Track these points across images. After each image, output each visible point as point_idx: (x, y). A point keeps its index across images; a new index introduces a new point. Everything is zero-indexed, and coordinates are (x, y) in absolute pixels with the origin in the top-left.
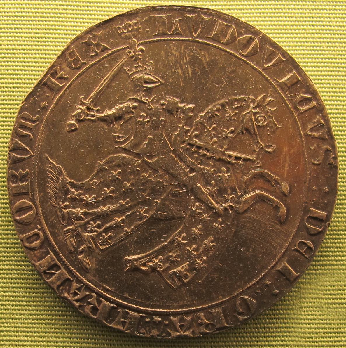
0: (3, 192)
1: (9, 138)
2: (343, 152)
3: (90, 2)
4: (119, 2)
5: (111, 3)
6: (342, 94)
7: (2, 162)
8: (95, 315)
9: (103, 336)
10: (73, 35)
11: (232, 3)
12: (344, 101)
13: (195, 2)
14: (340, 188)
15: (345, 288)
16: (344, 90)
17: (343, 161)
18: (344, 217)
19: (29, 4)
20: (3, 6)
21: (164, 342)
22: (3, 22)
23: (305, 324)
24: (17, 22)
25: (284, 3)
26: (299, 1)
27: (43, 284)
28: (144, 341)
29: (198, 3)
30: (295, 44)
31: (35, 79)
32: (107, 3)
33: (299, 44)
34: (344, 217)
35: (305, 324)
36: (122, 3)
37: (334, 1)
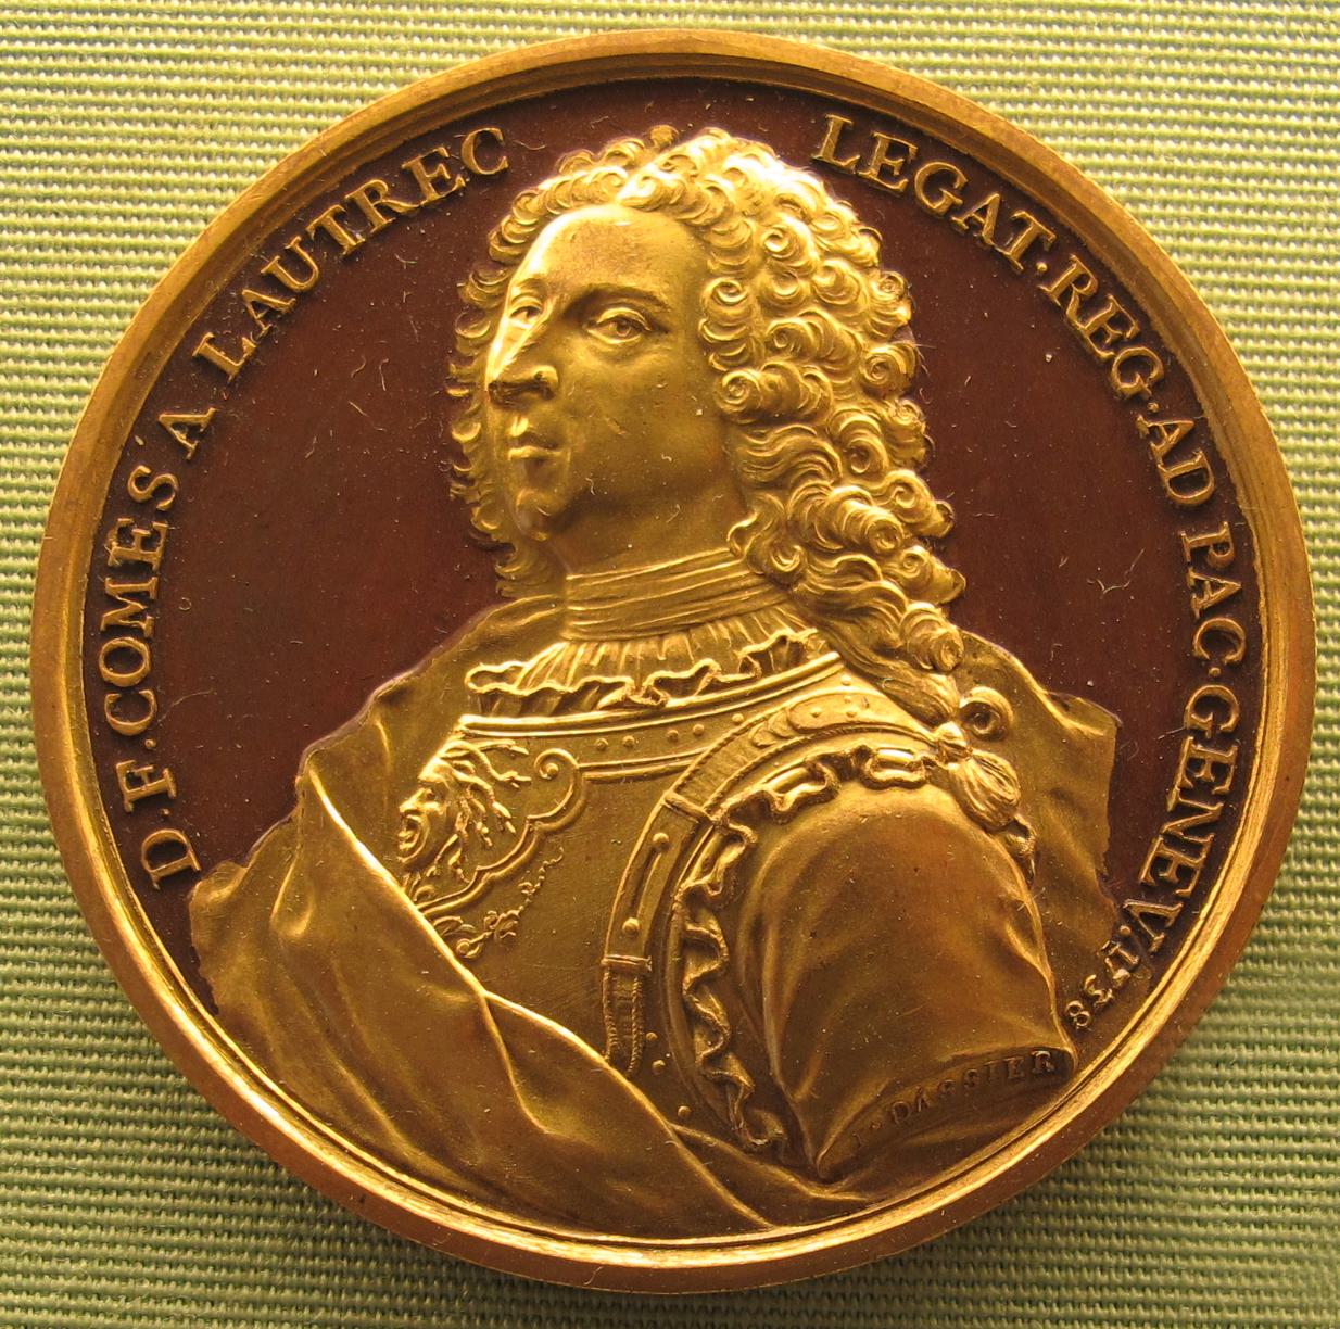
1: (80, 408)
2: (1325, 791)
3: (1071, 9)
6: (1326, 266)
7: (8, 1107)
8: (1083, 322)
10: (288, 143)
12: (1331, 1156)
14: (1321, 727)
16: (1333, 348)
17: (1329, 587)
18: (1334, 911)
19: (871, 18)
20: (12, 30)
21: (656, 1308)
23: (1203, 1153)
25: (309, 7)
26: (1317, 5)
28: (573, 1304)
30: (1177, 130)
33: (1191, 131)
34: (1334, 911)
35: (1203, 1153)
37: (442, 5)
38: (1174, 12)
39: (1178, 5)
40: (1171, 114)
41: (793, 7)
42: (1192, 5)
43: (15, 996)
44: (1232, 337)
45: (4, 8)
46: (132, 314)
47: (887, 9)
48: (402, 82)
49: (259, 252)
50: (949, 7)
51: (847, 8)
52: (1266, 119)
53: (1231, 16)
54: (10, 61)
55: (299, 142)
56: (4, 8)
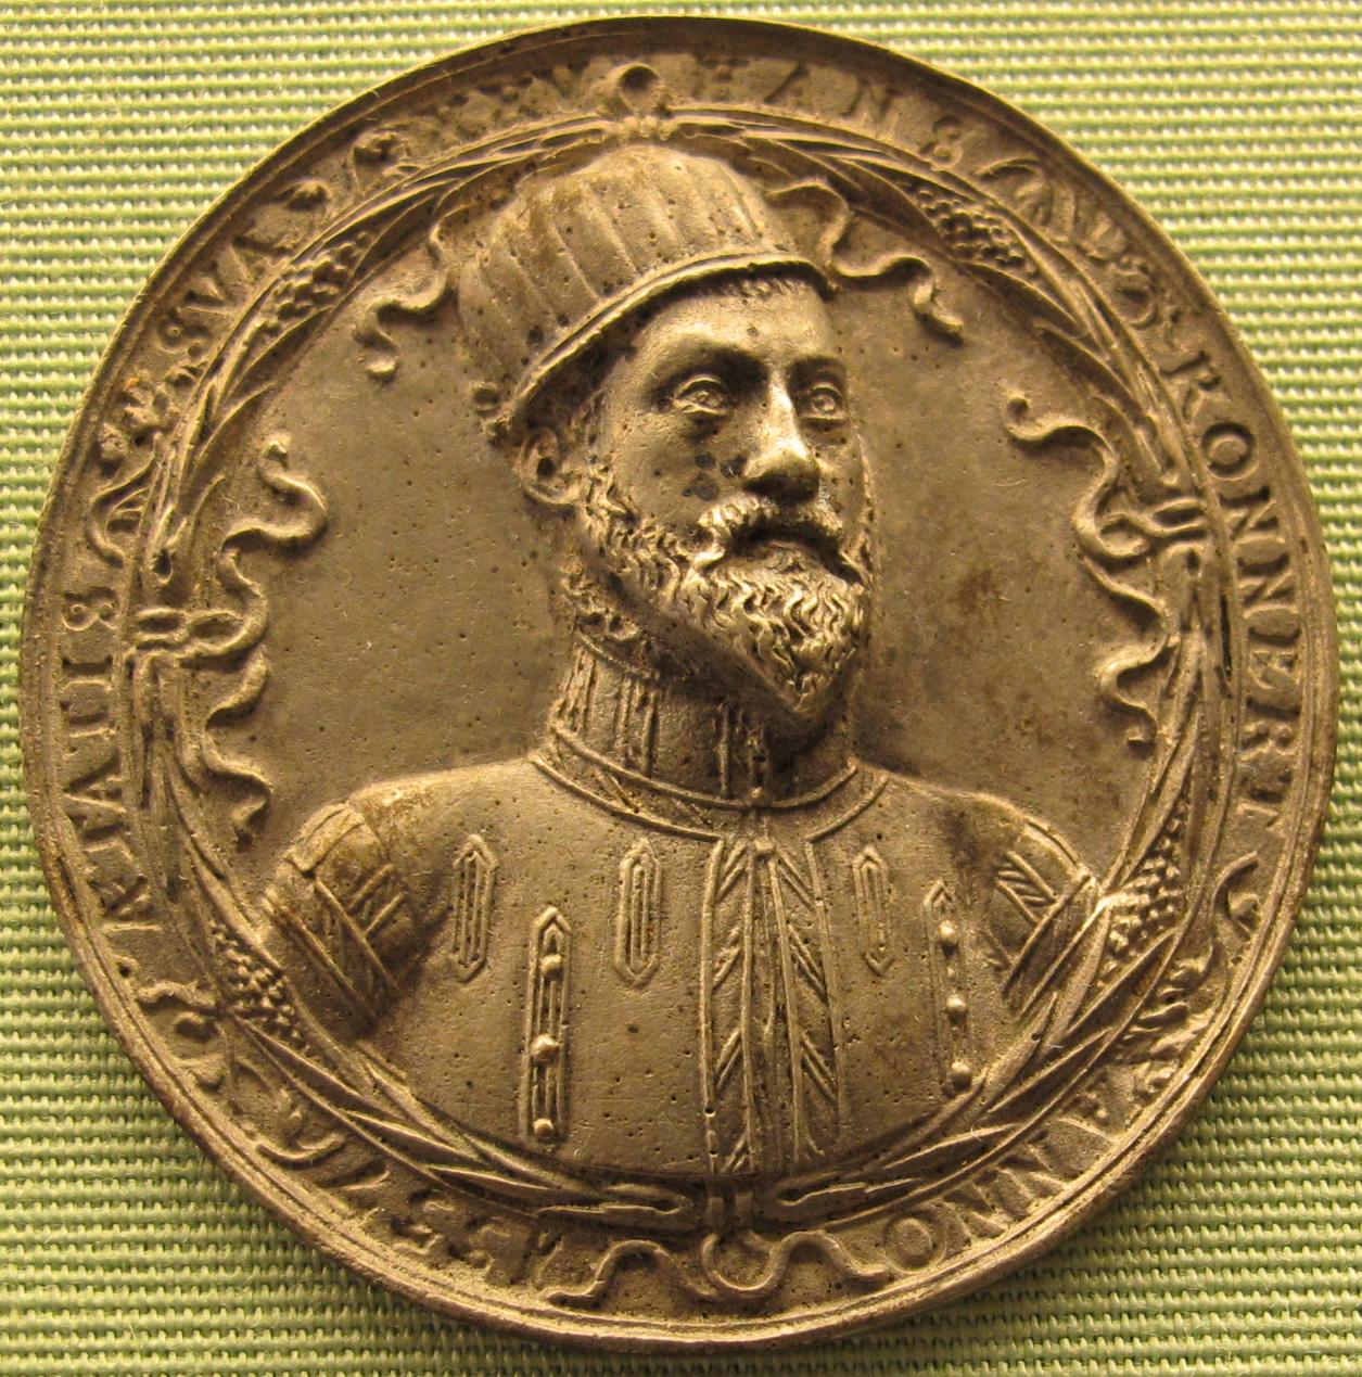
0: (14, 398)
4: (412, 6)
5: (481, 12)
9: (412, 1332)
11: (889, 10)
13: (749, 6)
15: (1355, 1106)
22: (14, 246)
24: (34, 31)
25: (857, 10)
26: (781, 5)
27: (140, 1096)
29: (794, 12)
31: (133, 275)
32: (464, 11)
36: (400, 14)
38: (1316, 14)
39: (1321, 6)
40: (1237, 114)
41: (308, 8)
42: (1337, 6)
43: (16, 149)
44: (1207, 273)
45: (7, 7)
46: (58, 447)
47: (199, 11)
48: (318, 105)
49: (968, 1242)
50: (97, 9)
51: (261, 9)
52: (1269, 114)
53: (1113, 19)
54: (13, 473)
55: (211, 198)
56: (7, 7)
